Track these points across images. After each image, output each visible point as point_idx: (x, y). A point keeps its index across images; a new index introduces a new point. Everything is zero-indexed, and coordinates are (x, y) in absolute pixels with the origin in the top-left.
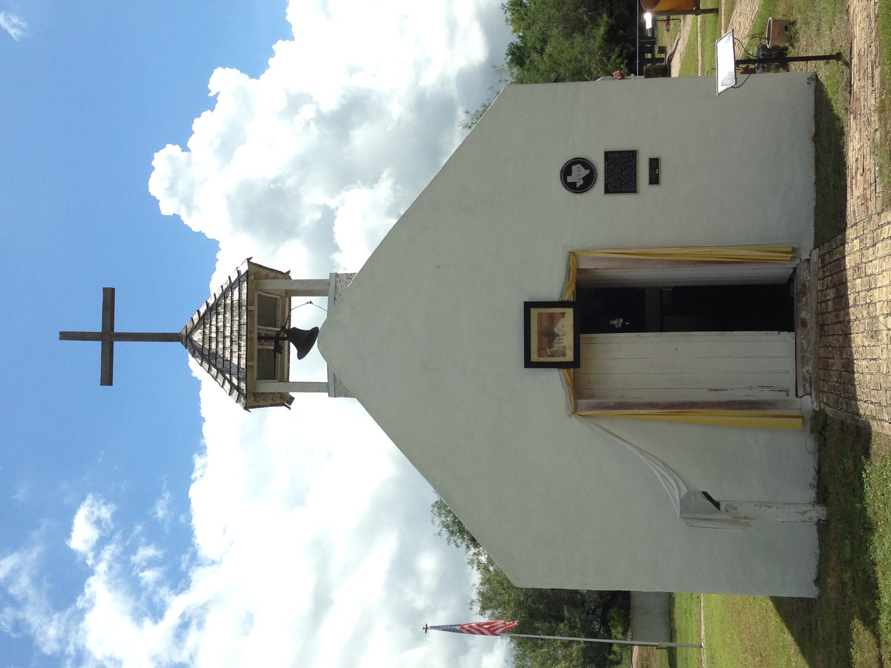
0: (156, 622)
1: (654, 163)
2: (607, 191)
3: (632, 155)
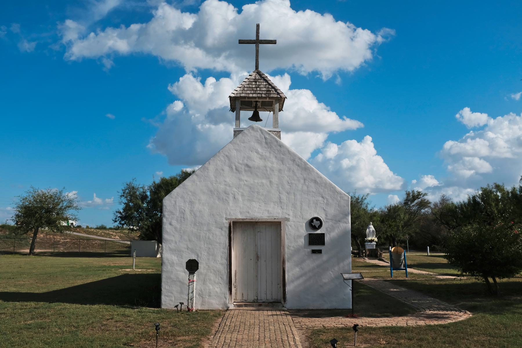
0: (282, 76)
1: (320, 252)
2: (310, 234)
3: (323, 243)
